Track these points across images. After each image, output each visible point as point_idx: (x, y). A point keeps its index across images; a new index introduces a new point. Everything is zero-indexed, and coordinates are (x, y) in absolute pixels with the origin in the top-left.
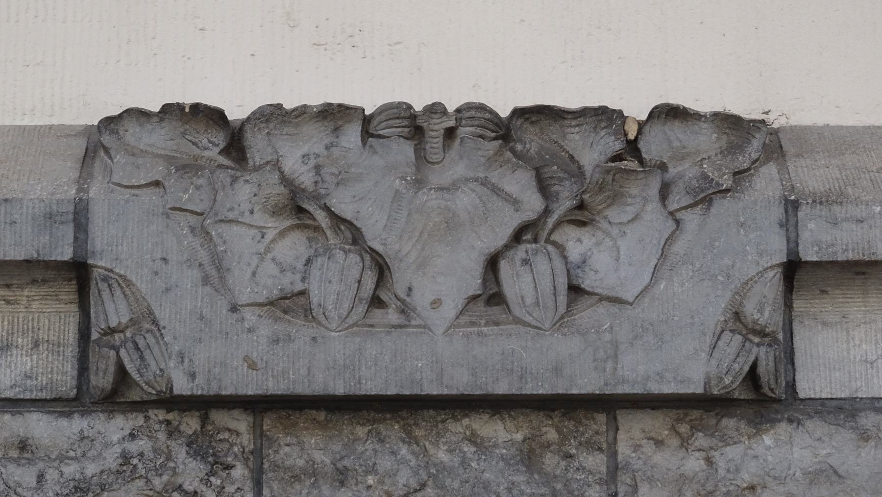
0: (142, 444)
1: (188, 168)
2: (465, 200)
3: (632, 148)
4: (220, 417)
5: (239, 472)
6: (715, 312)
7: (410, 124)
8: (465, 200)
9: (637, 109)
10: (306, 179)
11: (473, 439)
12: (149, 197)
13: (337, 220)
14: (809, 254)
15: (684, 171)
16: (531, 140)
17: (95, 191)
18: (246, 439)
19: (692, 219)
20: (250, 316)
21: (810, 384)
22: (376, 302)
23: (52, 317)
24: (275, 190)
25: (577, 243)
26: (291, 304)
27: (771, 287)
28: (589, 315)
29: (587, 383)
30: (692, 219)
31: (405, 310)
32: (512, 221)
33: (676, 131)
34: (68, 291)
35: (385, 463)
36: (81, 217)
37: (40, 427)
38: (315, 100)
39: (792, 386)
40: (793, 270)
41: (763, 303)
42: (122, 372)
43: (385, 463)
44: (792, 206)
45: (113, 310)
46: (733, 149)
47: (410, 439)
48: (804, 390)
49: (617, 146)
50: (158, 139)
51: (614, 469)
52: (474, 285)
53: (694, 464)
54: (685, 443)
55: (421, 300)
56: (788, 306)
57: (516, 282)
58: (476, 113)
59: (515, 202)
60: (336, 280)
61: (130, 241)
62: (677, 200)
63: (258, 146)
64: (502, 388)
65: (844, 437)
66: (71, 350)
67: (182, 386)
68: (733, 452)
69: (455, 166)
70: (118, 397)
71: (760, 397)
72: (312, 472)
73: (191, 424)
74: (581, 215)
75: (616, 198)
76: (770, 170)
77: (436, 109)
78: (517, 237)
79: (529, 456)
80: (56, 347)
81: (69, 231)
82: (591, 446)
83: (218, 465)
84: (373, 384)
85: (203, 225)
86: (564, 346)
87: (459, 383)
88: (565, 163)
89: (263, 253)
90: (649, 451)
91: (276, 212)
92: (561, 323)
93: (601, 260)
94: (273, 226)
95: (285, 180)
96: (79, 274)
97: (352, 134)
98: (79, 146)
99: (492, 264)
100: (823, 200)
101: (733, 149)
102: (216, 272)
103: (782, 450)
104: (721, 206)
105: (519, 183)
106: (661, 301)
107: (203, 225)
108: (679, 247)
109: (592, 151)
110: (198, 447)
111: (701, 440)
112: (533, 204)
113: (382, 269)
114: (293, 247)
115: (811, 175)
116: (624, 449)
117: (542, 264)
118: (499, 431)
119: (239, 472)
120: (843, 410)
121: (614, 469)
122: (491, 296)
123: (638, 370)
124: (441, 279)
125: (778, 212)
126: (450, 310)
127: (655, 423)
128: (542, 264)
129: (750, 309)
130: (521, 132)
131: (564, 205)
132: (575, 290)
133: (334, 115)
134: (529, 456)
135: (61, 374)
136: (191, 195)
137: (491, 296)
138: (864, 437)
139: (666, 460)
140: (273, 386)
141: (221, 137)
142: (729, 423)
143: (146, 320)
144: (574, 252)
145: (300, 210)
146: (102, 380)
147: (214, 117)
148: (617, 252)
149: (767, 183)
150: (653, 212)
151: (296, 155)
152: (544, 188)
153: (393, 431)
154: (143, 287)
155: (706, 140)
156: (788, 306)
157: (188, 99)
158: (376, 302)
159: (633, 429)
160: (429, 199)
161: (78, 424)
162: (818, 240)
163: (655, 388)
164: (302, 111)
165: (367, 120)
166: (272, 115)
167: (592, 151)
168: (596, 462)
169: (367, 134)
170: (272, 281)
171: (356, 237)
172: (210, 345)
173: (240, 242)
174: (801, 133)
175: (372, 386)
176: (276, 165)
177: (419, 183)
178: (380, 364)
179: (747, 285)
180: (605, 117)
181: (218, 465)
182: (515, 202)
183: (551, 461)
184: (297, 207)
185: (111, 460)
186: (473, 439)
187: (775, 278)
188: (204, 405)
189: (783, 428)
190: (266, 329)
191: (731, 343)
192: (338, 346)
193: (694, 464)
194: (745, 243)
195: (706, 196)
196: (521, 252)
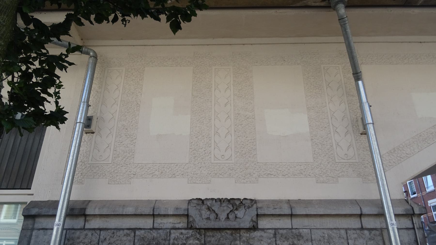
0: (193, 233)
1: (198, 205)
2: (225, 208)
3: (242, 202)
4: (201, 230)
5: (203, 236)
6: (250, 219)
7: (220, 200)
8: (225, 208)
9: (242, 198)
10: (210, 206)
11: (226, 232)
12: (194, 208)
13: (213, 210)
14: (259, 214)
15: (247, 205)
16: (232, 202)
17: (189, 207)
18: (204, 232)
19: (247, 210)
20: (204, 220)
21: (260, 227)
22: (217, 218)
23: (185, 220)
24: (207, 207)
25: (236, 212)
26: (208, 219)
27: (255, 217)
28: (238, 220)
29: (237, 227)
30: (247, 210)
31: (219, 219)
32: (230, 210)
33: (246, 201)
34: (186, 217)
35: (217, 235)
36: (188, 210)
37: (183, 231)
38: (211, 198)
39: (258, 227)
40: (257, 215)
41: (255, 219)
42: (191, 225)
43: (217, 235)
44: (257, 209)
45: (191, 219)
46: (252, 202)
47: (220, 233)
48: (259, 227)
49: (240, 202)
50: (195, 202)
51: (240, 236)
52: (226, 217)
53: (248, 235)
54: (247, 233)
55: (221, 218)
56: (257, 218)
57: (230, 216)
58: (226, 199)
59: (230, 208)
60: (213, 216)
61: (193, 212)
62: (246, 208)
63: (205, 202)
64: (229, 227)
65: (263, 232)
66: (186, 223)
67: (197, 227)
68: (252, 234)
69: (224, 204)
70: (191, 228)
71: (255, 228)
72: (210, 236)
73: (198, 231)
74: (237, 209)
75: (240, 208)
76: (255, 205)
77: (222, 199)
78: (230, 212)
79: (232, 234)
80: (185, 223)
81: (186, 211)
82: (238, 233)
83: (201, 235)
84: (216, 227)
85: (200, 210)
86: (235, 223)
87: (225, 227)
88: (235, 204)
89: (206, 213)
90: (245, 235)
91: (207, 209)
92: (235, 221)
93: (239, 214)
94: (206, 210)
95: (208, 206)
96: (187, 216)
97: (214, 201)
98: (188, 202)
99: (228, 214)
100: (261, 208)
101: (252, 202)
102: (201, 215)
103: (257, 234)
104: (250, 209)
105: (230, 206)
106: (245, 218)
107: (200, 210)
108: (246, 213)
109: (238, 203)
110: (199, 233)
111: (249, 233)
112: (232, 208)
113: (217, 215)
114: (208, 213)
115: (259, 205)
116: (241, 234)
117: (233, 215)
118: (229, 232)
119: (203, 236)
120: (263, 230)
121: (240, 236)
122: (228, 218)
123: (242, 225)
124: (223, 216)
125: (256, 209)
126: (224, 219)
127: (244, 231)
128: (233, 215)
129: (253, 219)
130: (230, 201)
131: (235, 208)
132: (236, 217)
133: (212, 199)
134: (232, 234)
135: (185, 225)
136: (199, 208)
137: (228, 218)
138: (265, 232)
139: (245, 235)
140: (206, 227)
141: (202, 201)
142: (251, 231)
143: (194, 220)
144: (236, 213)
145: (209, 209)
146: (190, 226)
147: (200, 199)
148: (240, 213)
149: (255, 206)
150: (244, 209)
151: (209, 203)
152: (233, 207)
153: (218, 232)
154: (194, 217)
155: (249, 202)
156: (257, 218)
157: (198, 198)
158: (217, 218)
159: (242, 232)
160: (222, 208)
161: (187, 231)
162: (260, 212)
163: (244, 227)
164: (209, 199)
165: (216, 199)
166: (206, 199)
167: (238, 203)
168: (238, 235)
169: (216, 201)
170: (206, 216)
171: (214, 212)
172: (201, 223)
173: (203, 212)
174: (258, 200)
175: (216, 227)
176: (207, 204)
177: (221, 206)
178: (217, 225)
179: (252, 217)
180: (239, 199)
181: (201, 235)
182: (230, 208)
183: (234, 235)
184: (209, 209)
185: (190, 235)
186: (226, 232)
187: (256, 216)
188: (199, 229)
189: (257, 231)
190: (206, 221)
191: (251, 223)
192: (213, 223)
193: (248, 235)
194: (253, 212)
195: (249, 207)
196: (231, 213)
